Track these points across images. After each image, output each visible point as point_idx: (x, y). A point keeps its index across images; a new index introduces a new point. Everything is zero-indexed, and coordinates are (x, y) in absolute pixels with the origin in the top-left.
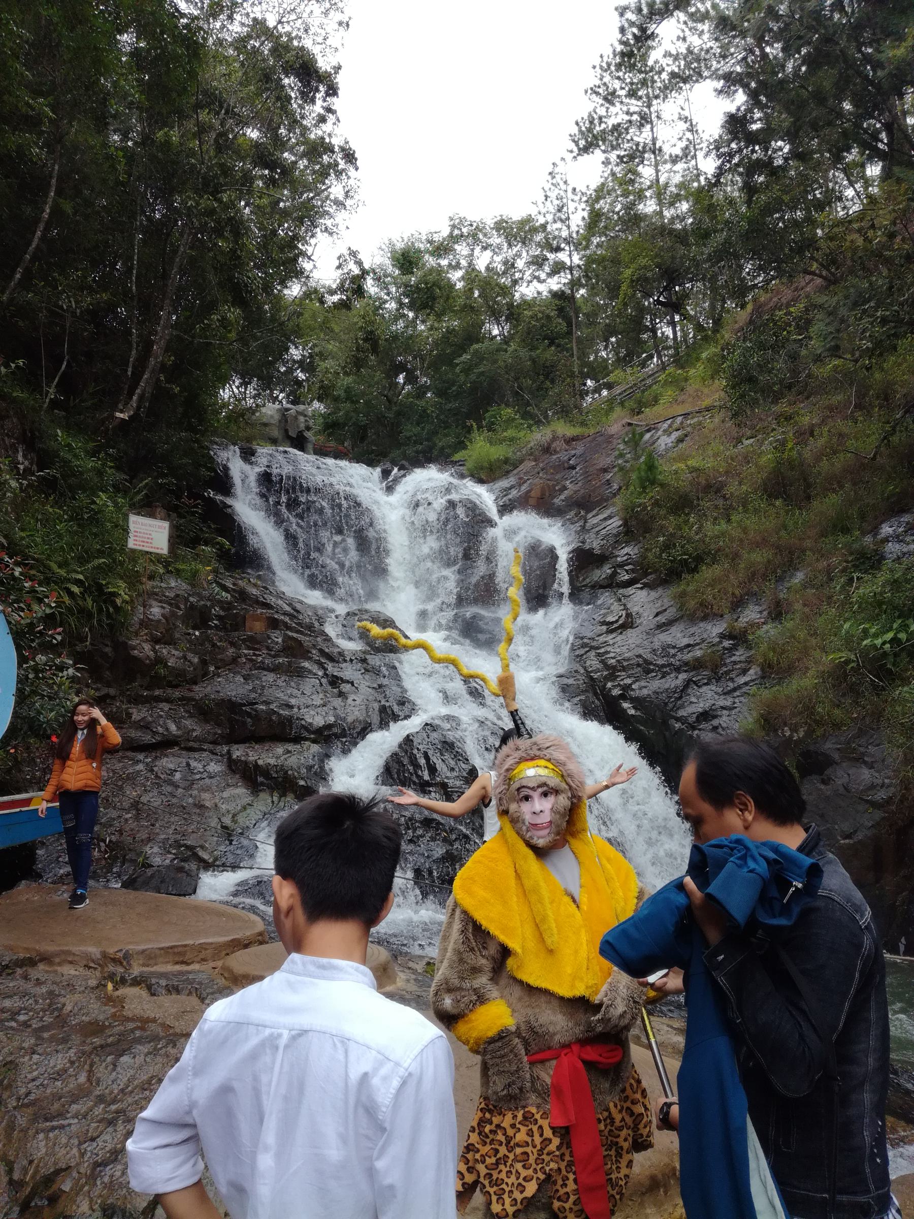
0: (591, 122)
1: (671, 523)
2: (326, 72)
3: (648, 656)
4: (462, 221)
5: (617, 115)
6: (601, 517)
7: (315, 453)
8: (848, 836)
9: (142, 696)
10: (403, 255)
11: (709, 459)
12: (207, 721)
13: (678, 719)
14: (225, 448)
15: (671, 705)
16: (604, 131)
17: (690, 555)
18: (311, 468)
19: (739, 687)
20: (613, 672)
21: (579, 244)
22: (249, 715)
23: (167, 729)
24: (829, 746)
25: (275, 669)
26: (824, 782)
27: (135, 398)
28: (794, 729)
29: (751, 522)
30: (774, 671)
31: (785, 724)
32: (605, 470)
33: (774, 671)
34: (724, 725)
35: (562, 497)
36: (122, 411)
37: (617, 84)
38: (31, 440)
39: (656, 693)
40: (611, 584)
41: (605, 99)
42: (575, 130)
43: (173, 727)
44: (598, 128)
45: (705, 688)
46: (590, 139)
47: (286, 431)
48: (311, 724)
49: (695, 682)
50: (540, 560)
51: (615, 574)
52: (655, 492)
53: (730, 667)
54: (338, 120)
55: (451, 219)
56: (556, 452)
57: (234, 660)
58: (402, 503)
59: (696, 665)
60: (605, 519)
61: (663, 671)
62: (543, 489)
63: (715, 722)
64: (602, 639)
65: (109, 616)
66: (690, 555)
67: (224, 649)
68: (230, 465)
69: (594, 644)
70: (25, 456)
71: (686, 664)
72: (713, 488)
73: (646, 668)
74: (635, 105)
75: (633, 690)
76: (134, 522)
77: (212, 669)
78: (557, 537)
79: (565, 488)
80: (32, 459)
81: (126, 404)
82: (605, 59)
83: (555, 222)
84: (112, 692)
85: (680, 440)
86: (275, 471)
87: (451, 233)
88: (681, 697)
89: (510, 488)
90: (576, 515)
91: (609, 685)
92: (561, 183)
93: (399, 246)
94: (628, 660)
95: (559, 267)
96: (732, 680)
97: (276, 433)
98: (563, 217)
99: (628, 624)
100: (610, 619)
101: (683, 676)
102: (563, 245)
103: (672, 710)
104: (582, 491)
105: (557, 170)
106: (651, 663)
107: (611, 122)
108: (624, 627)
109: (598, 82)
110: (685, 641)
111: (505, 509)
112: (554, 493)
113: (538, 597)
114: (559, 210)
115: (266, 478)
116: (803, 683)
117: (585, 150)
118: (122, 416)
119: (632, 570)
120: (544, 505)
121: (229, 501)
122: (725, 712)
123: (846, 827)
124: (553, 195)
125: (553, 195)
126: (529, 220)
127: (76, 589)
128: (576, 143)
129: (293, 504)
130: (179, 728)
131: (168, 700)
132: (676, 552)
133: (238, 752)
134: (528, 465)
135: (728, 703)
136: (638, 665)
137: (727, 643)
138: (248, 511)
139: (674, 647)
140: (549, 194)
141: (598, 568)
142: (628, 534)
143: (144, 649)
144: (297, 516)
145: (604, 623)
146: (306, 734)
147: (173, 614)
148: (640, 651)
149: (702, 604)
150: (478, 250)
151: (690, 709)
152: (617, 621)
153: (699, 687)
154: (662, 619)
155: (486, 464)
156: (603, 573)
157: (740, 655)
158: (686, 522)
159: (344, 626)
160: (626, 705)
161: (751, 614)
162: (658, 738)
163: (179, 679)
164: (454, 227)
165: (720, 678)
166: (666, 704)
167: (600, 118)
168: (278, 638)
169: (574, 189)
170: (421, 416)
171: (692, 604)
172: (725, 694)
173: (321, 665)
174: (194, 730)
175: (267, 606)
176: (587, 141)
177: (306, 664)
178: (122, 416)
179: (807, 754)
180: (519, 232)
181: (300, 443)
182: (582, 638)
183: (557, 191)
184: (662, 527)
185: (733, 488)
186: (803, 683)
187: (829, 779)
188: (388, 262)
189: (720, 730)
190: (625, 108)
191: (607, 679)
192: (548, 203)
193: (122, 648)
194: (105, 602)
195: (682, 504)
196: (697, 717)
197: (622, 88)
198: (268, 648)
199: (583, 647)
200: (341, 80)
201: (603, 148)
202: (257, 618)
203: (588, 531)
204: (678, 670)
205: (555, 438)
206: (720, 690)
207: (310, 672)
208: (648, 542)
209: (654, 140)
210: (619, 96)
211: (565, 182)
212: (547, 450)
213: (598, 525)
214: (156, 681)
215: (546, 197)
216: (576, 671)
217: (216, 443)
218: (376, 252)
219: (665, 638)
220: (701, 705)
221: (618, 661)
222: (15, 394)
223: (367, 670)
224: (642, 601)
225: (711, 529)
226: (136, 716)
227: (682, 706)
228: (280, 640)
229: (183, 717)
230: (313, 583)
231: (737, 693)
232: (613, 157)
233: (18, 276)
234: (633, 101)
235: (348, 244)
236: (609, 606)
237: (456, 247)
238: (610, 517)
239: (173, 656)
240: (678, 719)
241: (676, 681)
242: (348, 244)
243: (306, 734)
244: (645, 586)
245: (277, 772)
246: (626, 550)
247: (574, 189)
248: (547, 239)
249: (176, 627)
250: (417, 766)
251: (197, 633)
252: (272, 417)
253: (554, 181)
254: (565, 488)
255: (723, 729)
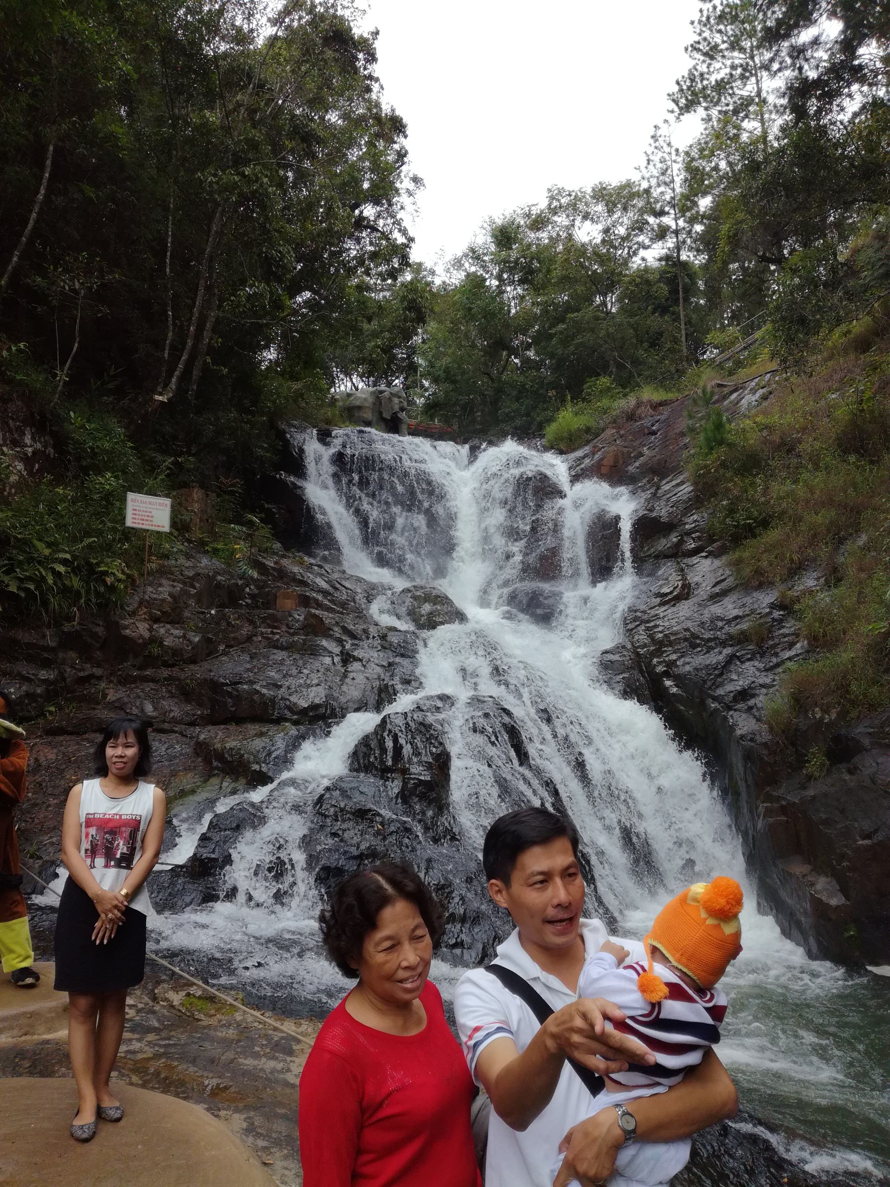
0: (692, 80)
1: (735, 485)
2: (361, 37)
3: (695, 629)
4: (560, 192)
5: (719, 71)
6: (674, 483)
7: (409, 434)
8: (868, 836)
9: (131, 676)
10: (501, 231)
11: (785, 417)
12: (188, 701)
13: (715, 699)
14: (303, 430)
15: (709, 683)
16: (704, 88)
17: (755, 519)
18: (386, 445)
19: (783, 662)
20: (660, 645)
21: (685, 204)
22: (230, 695)
23: (142, 710)
24: (860, 731)
25: (288, 648)
26: (850, 772)
27: (174, 380)
28: (826, 711)
29: (818, 480)
30: (821, 642)
31: (816, 705)
32: (682, 434)
33: (821, 642)
34: (759, 705)
35: (637, 464)
36: (161, 394)
37: (718, 38)
38: (43, 423)
39: (696, 669)
40: (676, 554)
41: (705, 54)
42: (676, 88)
43: (149, 708)
44: (700, 86)
45: (747, 664)
46: (691, 96)
47: (381, 413)
48: (295, 704)
49: (738, 657)
50: (604, 531)
51: (681, 542)
52: (722, 452)
53: (777, 641)
54: (382, 88)
55: (549, 190)
56: (641, 418)
57: (249, 639)
58: (468, 477)
59: (741, 639)
60: (678, 485)
61: (708, 645)
62: (616, 456)
63: (751, 702)
64: (653, 612)
65: (98, 594)
66: (755, 519)
67: (238, 628)
68: (305, 447)
69: (646, 617)
70: (33, 439)
71: (731, 637)
72: (787, 447)
73: (693, 642)
74: (738, 57)
75: (677, 666)
76: (132, 500)
77: (222, 647)
78: (625, 506)
79: (641, 455)
80: (46, 441)
81: (166, 385)
82: (705, 13)
83: (659, 185)
84: (98, 672)
85: (765, 398)
86: (348, 451)
87: (550, 205)
88: (721, 674)
89: (584, 458)
90: (649, 482)
91: (655, 660)
92: (665, 146)
93: (499, 222)
94: (676, 634)
95: (662, 233)
96: (776, 655)
97: (368, 415)
98: (667, 180)
99: (685, 593)
100: (666, 590)
101: (728, 651)
102: (667, 209)
103: (710, 688)
104: (658, 457)
105: (659, 133)
106: (698, 637)
107: (713, 78)
108: (678, 599)
109: (697, 38)
110: (735, 612)
111: (575, 479)
112: (627, 459)
113: (603, 568)
114: (663, 174)
115: (339, 459)
116: (847, 655)
117: (689, 107)
118: (160, 398)
119: (698, 537)
120: (614, 474)
121: (299, 483)
122: (764, 691)
123: (866, 825)
124: (656, 158)
125: (656, 158)
126: (629, 184)
127: (61, 569)
128: (676, 102)
129: (364, 483)
130: (155, 709)
131: (153, 681)
132: (741, 516)
133: (204, 734)
134: (610, 432)
135: (768, 681)
136: (686, 639)
137: (777, 614)
138: (322, 495)
139: (722, 620)
140: (651, 157)
141: (664, 536)
142: (696, 502)
143: (139, 628)
144: (367, 495)
145: (659, 595)
146: (288, 714)
147: (184, 592)
148: (689, 624)
149: (758, 572)
150: (579, 219)
151: (730, 687)
152: (671, 592)
153: (742, 663)
154: (717, 589)
155: (565, 435)
156: (664, 544)
157: (790, 626)
158: (753, 484)
159: (393, 603)
160: (668, 683)
161: (809, 581)
162: (692, 720)
163: (176, 658)
164: (552, 198)
165: (765, 653)
166: (705, 682)
167: (702, 75)
168: (300, 616)
169: (677, 150)
170: (520, 392)
171: (747, 571)
172: (766, 670)
173: (340, 642)
174: (171, 711)
175: (303, 583)
176: (687, 99)
177: (324, 643)
178: (160, 398)
179: (837, 739)
180: (615, 198)
181: (393, 425)
182: (636, 611)
183: (660, 154)
184: (728, 490)
185: (808, 445)
186: (847, 655)
187: (856, 768)
188: (489, 239)
189: (754, 710)
190: (728, 63)
191: (653, 654)
192: (651, 167)
193: (114, 627)
194: (96, 580)
195: (750, 464)
196: (735, 697)
197: (724, 42)
198: (287, 626)
199: (634, 620)
200: (380, 46)
201: (704, 104)
202: (287, 596)
203: (659, 498)
204: (724, 644)
205: (639, 404)
206: (762, 666)
207: (325, 649)
208: (712, 510)
209: (759, 94)
210: (721, 51)
211: (669, 144)
212: (631, 416)
213: (669, 491)
214: (151, 661)
215: (649, 161)
216: (624, 647)
217: (294, 426)
218: (478, 231)
219: (716, 609)
220: (741, 683)
221: (666, 635)
222: (18, 377)
223: (384, 647)
224: (705, 571)
225: (779, 489)
226: (112, 696)
227: (722, 685)
228: (302, 618)
229: (163, 698)
230: (381, 561)
231: (780, 670)
232: (714, 112)
233: (15, 259)
234: (736, 54)
235: (443, 222)
236: (668, 577)
237: (556, 218)
238: (682, 483)
239: (171, 636)
240: (715, 699)
241: (716, 657)
242: (443, 222)
243: (288, 714)
244: (710, 554)
245: (232, 756)
246: (695, 517)
247: (677, 150)
248: (649, 203)
249: (187, 606)
250: (384, 750)
251: (213, 612)
252: (365, 399)
253: (657, 144)
254: (641, 455)
255: (758, 709)
